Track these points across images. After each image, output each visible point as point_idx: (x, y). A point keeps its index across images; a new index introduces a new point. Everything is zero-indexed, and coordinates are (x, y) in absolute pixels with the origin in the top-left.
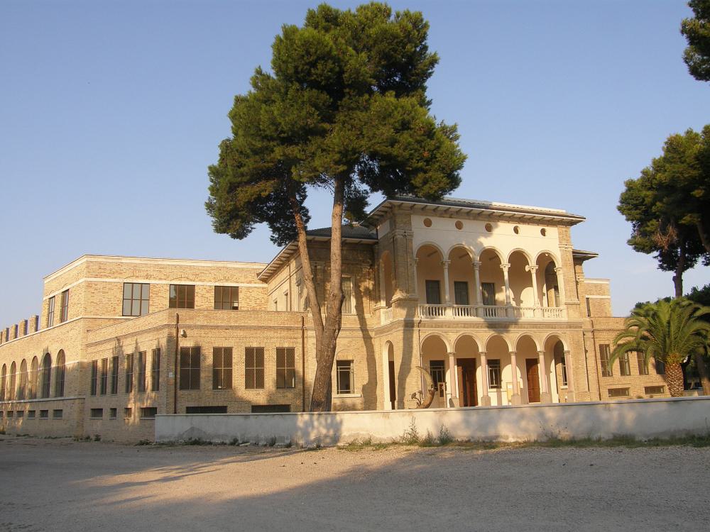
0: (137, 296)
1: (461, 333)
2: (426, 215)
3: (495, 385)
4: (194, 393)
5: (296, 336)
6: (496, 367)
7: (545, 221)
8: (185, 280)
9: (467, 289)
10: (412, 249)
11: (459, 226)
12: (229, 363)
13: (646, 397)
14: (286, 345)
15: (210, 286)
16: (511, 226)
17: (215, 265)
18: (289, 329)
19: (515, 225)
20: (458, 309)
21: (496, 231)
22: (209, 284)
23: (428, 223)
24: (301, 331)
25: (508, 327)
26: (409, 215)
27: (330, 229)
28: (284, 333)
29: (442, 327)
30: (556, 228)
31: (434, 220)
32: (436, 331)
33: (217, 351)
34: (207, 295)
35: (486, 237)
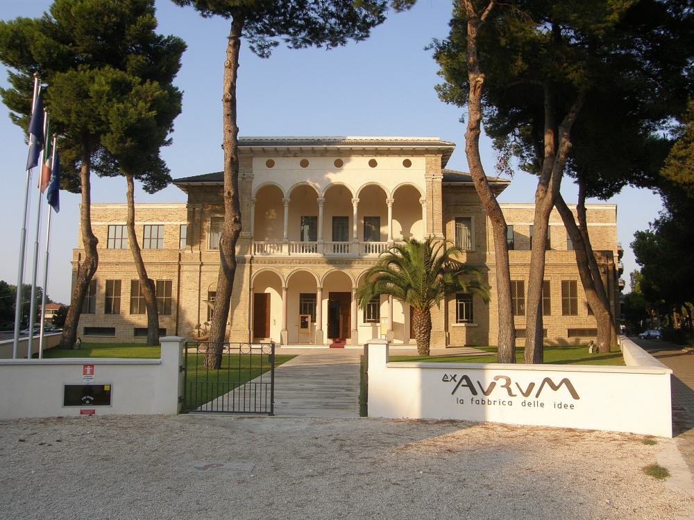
0: (154, 235)
1: (296, 268)
2: (269, 157)
3: (372, 319)
4: (90, 316)
5: (173, 270)
6: (311, 301)
7: (408, 152)
8: (156, 221)
9: (379, 221)
10: (251, 190)
11: (373, 164)
12: (118, 292)
13: (571, 340)
14: (165, 278)
15: (177, 225)
16: (366, 160)
17: (181, 207)
18: (167, 264)
19: (267, 159)
20: (296, 245)
21: (347, 166)
22: (175, 223)
23: (270, 164)
24: (177, 266)
25: (351, 263)
26: (251, 158)
27: (223, 172)
28: (164, 268)
29: (276, 262)
30: (424, 158)
31: (276, 160)
32: (270, 267)
33: (109, 283)
34: (174, 233)
35: (334, 172)
